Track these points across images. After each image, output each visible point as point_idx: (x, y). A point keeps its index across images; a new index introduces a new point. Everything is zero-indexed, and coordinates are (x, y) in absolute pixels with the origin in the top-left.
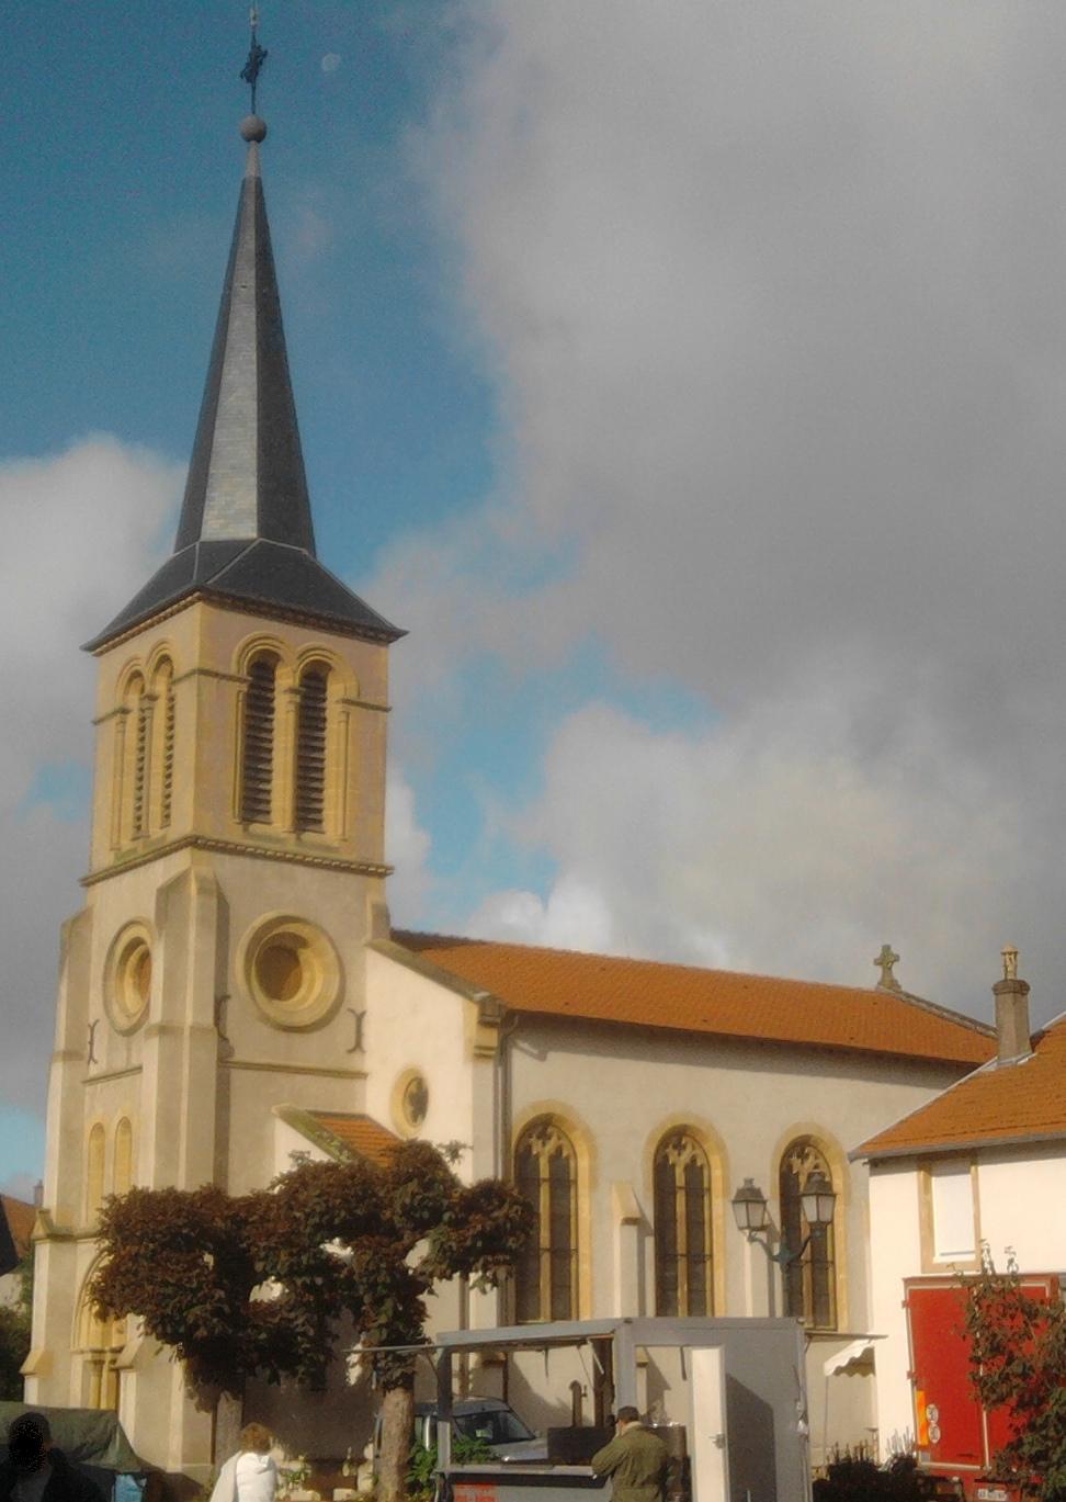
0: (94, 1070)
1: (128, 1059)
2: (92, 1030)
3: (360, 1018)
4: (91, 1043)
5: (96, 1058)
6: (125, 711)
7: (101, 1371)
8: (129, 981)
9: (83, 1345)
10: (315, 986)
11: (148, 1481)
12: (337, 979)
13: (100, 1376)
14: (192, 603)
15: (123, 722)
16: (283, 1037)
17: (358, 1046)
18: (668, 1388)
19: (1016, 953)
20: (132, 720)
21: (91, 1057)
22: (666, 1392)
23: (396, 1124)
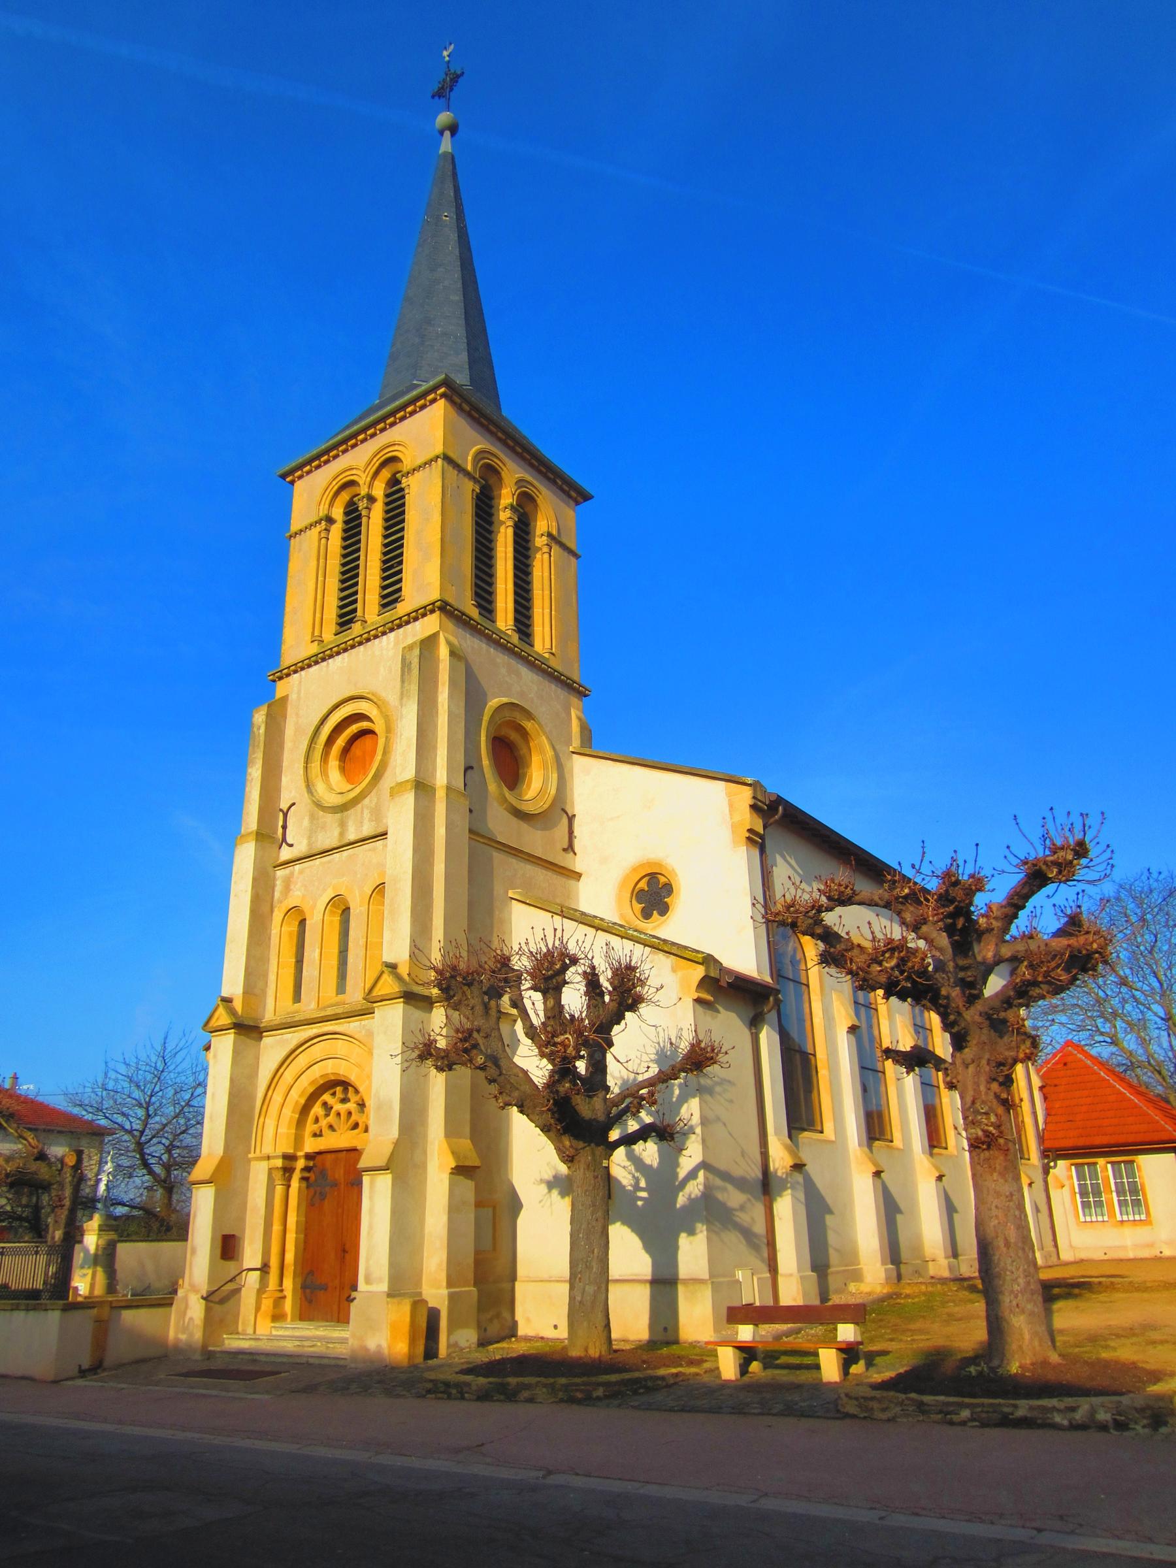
0: (286, 854)
1: (342, 834)
2: (285, 815)
3: (571, 819)
4: (284, 827)
5: (289, 840)
6: (330, 520)
7: (289, 1179)
8: (334, 763)
9: (268, 1149)
10: (537, 783)
11: (579, 1076)
12: (555, 776)
13: (289, 1186)
14: (434, 401)
15: (327, 530)
16: (514, 821)
17: (570, 848)
18: (830, 1212)
19: (1082, 814)
20: (337, 531)
21: (284, 839)
22: (828, 1218)
23: (622, 916)
